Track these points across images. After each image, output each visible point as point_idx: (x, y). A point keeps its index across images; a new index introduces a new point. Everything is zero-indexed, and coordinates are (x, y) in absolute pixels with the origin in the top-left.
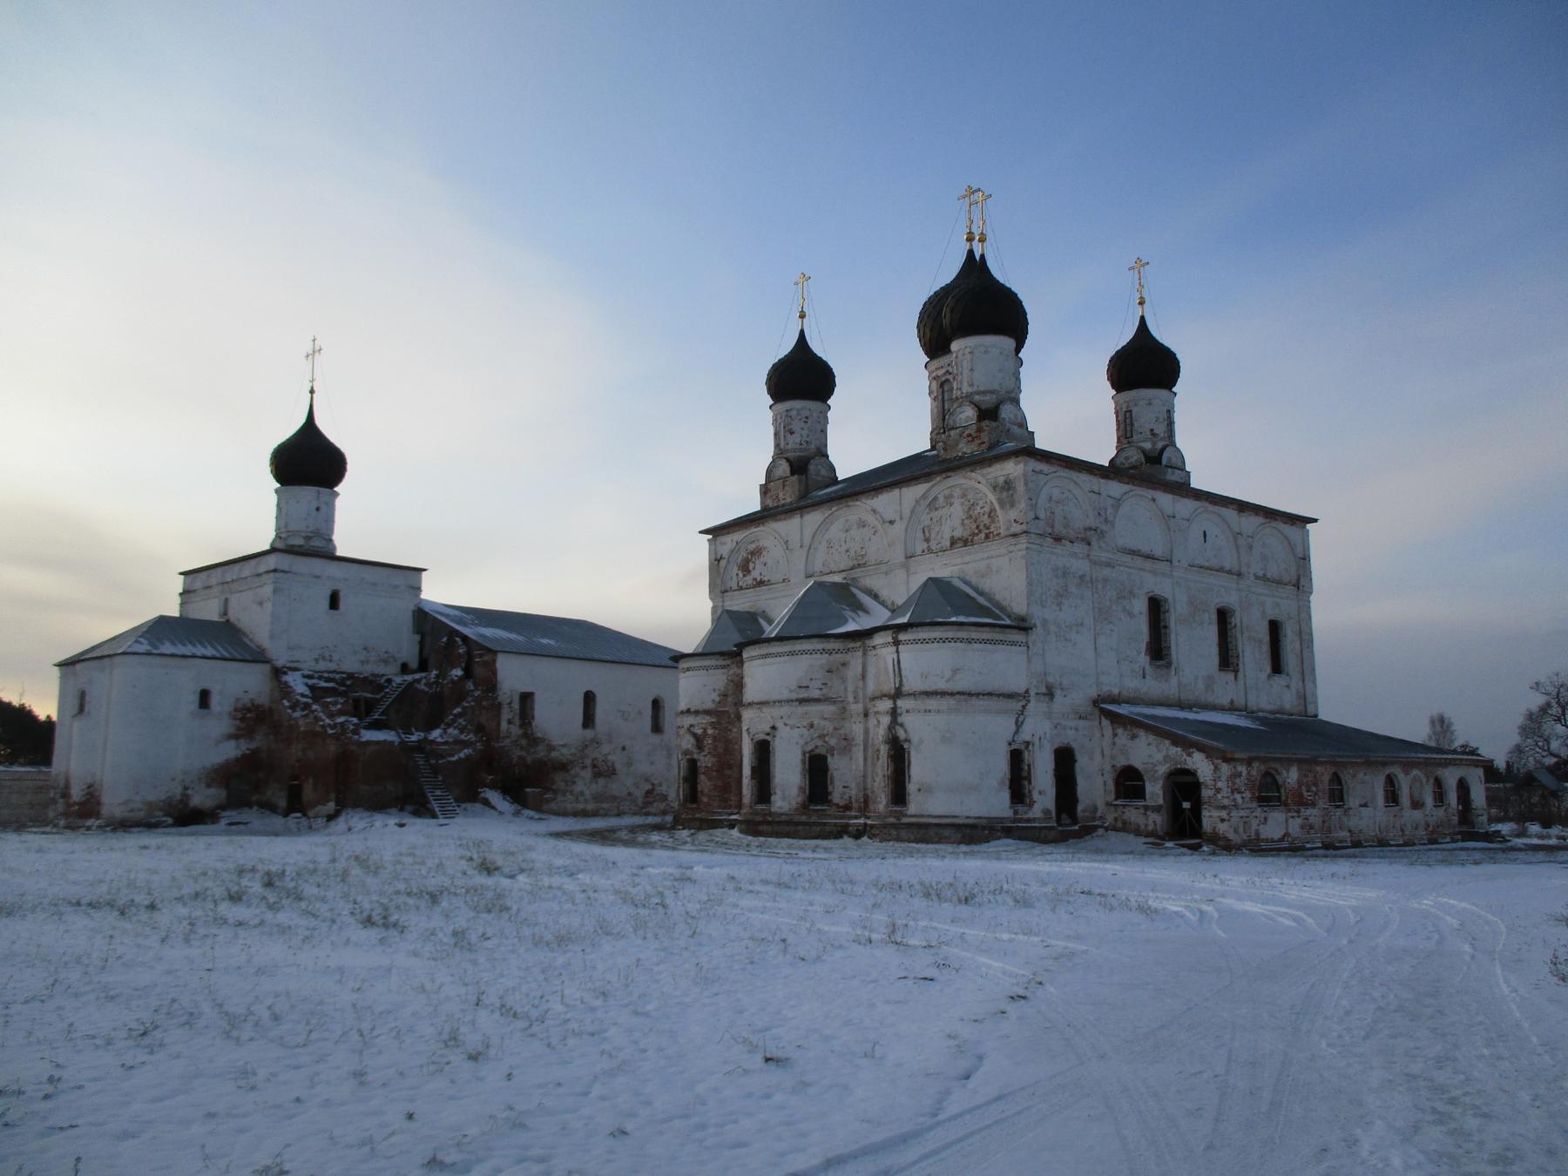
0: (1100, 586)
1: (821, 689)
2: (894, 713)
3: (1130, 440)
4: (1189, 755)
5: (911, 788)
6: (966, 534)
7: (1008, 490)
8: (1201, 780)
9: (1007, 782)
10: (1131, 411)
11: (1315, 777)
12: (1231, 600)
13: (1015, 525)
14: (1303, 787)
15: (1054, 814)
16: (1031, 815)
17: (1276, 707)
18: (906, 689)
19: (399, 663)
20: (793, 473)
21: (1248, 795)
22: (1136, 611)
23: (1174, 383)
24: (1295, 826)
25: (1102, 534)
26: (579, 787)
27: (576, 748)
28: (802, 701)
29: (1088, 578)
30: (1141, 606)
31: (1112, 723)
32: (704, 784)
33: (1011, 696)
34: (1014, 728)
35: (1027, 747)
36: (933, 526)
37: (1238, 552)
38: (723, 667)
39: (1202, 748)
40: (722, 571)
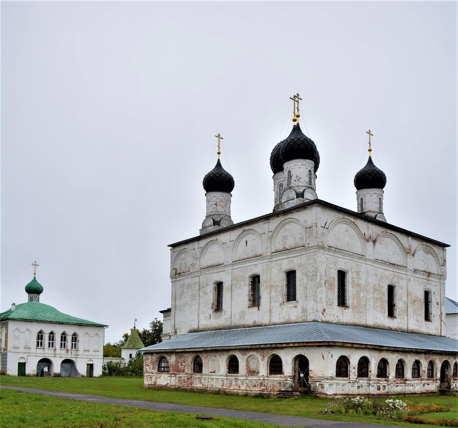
0: (193, 286)
19: (370, 149)
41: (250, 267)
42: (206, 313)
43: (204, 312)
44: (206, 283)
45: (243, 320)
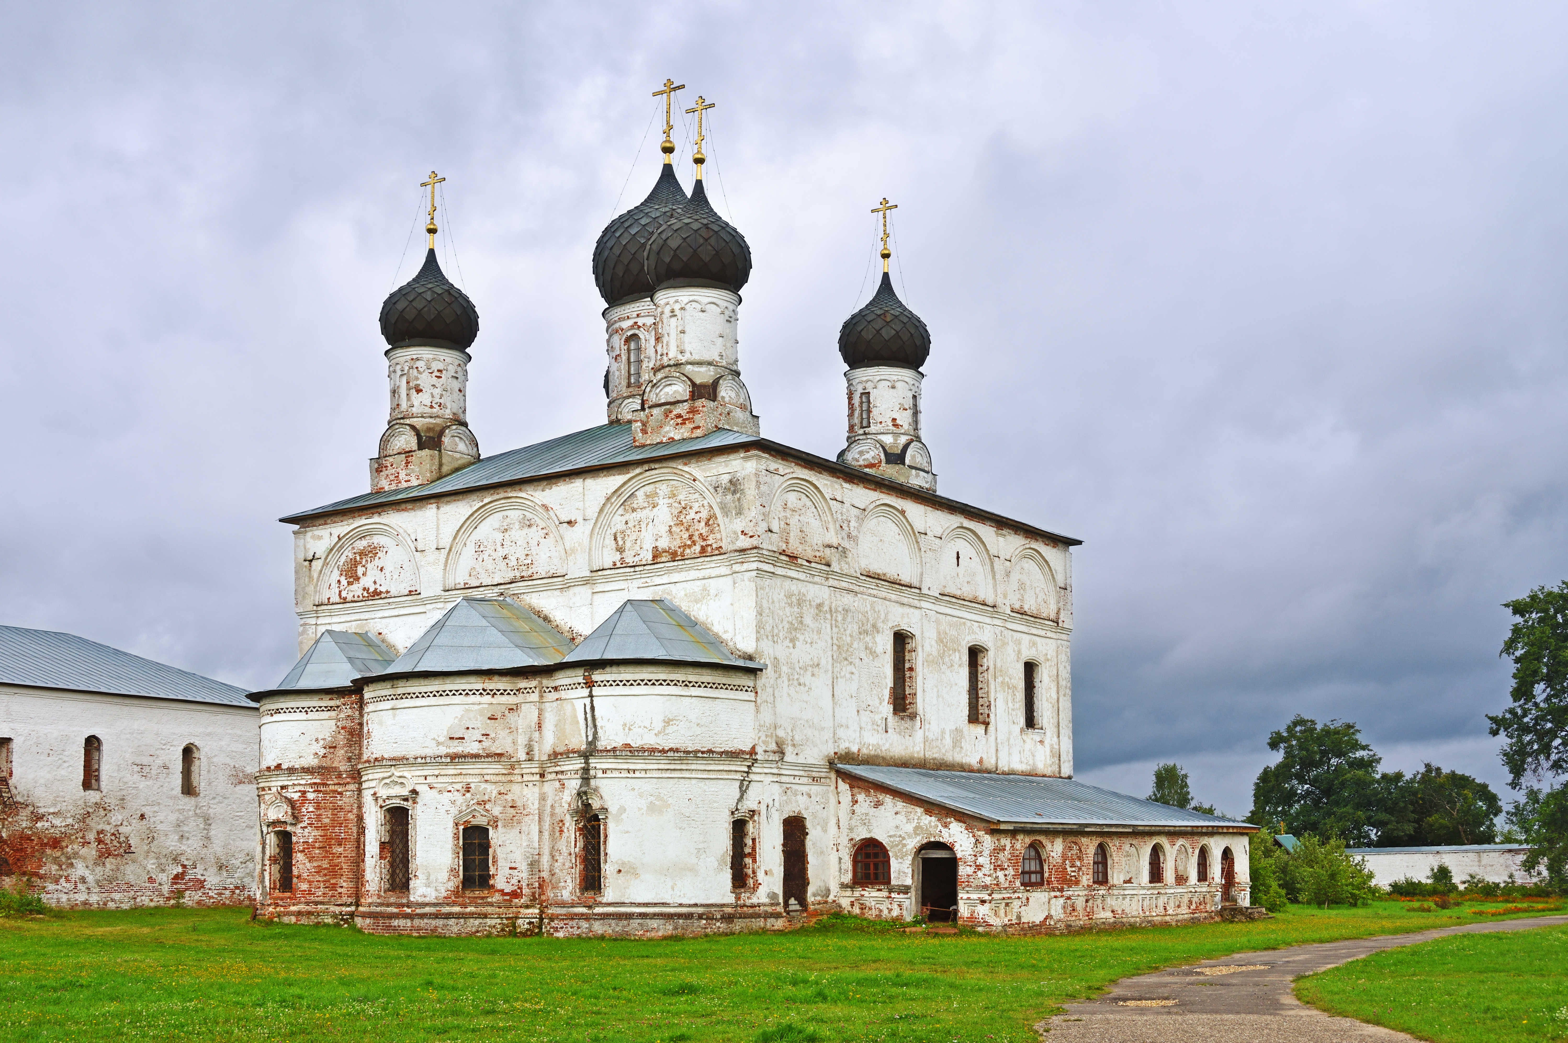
0: (840, 618)
1: (480, 741)
2: (586, 776)
3: (867, 430)
4: (946, 826)
5: (608, 869)
6: (675, 545)
7: (734, 492)
8: (959, 856)
9: (729, 860)
10: (869, 393)
11: (1080, 850)
12: (984, 637)
13: (743, 537)
14: (1067, 862)
15: (781, 900)
16: (754, 900)
17: (1029, 768)
18: (601, 745)
20: (421, 446)
21: (1011, 871)
22: (879, 649)
23: (740, 286)
24: (1057, 909)
25: (844, 552)
26: (80, 869)
27: (74, 817)
28: (455, 758)
29: (826, 608)
30: (885, 643)
31: (851, 787)
32: (301, 864)
33: (733, 755)
34: (737, 795)
35: (752, 817)
36: (628, 532)
37: (994, 577)
38: (331, 709)
39: (961, 816)
40: (315, 575)
41: (968, 623)
42: (878, 713)
43: (870, 708)
44: (871, 621)
45: (960, 752)
